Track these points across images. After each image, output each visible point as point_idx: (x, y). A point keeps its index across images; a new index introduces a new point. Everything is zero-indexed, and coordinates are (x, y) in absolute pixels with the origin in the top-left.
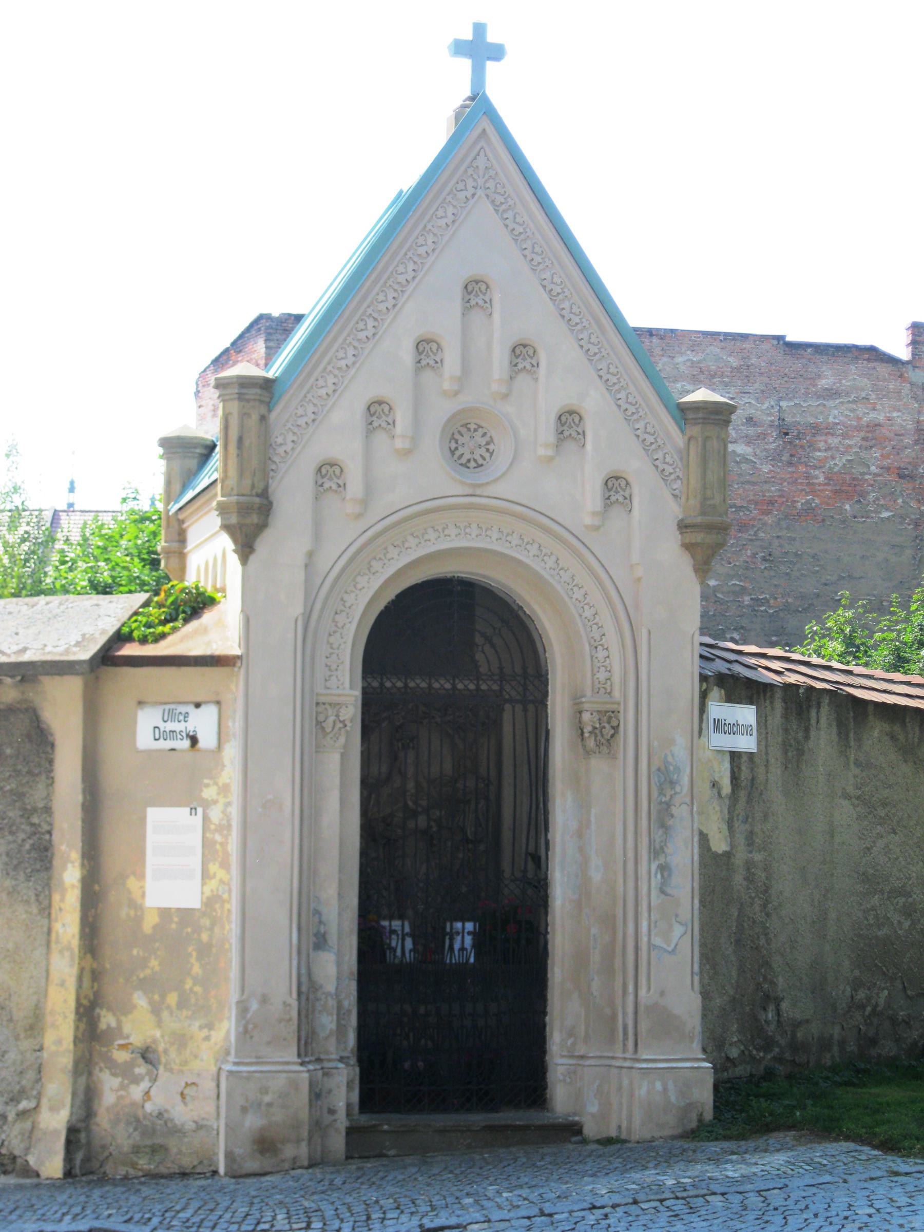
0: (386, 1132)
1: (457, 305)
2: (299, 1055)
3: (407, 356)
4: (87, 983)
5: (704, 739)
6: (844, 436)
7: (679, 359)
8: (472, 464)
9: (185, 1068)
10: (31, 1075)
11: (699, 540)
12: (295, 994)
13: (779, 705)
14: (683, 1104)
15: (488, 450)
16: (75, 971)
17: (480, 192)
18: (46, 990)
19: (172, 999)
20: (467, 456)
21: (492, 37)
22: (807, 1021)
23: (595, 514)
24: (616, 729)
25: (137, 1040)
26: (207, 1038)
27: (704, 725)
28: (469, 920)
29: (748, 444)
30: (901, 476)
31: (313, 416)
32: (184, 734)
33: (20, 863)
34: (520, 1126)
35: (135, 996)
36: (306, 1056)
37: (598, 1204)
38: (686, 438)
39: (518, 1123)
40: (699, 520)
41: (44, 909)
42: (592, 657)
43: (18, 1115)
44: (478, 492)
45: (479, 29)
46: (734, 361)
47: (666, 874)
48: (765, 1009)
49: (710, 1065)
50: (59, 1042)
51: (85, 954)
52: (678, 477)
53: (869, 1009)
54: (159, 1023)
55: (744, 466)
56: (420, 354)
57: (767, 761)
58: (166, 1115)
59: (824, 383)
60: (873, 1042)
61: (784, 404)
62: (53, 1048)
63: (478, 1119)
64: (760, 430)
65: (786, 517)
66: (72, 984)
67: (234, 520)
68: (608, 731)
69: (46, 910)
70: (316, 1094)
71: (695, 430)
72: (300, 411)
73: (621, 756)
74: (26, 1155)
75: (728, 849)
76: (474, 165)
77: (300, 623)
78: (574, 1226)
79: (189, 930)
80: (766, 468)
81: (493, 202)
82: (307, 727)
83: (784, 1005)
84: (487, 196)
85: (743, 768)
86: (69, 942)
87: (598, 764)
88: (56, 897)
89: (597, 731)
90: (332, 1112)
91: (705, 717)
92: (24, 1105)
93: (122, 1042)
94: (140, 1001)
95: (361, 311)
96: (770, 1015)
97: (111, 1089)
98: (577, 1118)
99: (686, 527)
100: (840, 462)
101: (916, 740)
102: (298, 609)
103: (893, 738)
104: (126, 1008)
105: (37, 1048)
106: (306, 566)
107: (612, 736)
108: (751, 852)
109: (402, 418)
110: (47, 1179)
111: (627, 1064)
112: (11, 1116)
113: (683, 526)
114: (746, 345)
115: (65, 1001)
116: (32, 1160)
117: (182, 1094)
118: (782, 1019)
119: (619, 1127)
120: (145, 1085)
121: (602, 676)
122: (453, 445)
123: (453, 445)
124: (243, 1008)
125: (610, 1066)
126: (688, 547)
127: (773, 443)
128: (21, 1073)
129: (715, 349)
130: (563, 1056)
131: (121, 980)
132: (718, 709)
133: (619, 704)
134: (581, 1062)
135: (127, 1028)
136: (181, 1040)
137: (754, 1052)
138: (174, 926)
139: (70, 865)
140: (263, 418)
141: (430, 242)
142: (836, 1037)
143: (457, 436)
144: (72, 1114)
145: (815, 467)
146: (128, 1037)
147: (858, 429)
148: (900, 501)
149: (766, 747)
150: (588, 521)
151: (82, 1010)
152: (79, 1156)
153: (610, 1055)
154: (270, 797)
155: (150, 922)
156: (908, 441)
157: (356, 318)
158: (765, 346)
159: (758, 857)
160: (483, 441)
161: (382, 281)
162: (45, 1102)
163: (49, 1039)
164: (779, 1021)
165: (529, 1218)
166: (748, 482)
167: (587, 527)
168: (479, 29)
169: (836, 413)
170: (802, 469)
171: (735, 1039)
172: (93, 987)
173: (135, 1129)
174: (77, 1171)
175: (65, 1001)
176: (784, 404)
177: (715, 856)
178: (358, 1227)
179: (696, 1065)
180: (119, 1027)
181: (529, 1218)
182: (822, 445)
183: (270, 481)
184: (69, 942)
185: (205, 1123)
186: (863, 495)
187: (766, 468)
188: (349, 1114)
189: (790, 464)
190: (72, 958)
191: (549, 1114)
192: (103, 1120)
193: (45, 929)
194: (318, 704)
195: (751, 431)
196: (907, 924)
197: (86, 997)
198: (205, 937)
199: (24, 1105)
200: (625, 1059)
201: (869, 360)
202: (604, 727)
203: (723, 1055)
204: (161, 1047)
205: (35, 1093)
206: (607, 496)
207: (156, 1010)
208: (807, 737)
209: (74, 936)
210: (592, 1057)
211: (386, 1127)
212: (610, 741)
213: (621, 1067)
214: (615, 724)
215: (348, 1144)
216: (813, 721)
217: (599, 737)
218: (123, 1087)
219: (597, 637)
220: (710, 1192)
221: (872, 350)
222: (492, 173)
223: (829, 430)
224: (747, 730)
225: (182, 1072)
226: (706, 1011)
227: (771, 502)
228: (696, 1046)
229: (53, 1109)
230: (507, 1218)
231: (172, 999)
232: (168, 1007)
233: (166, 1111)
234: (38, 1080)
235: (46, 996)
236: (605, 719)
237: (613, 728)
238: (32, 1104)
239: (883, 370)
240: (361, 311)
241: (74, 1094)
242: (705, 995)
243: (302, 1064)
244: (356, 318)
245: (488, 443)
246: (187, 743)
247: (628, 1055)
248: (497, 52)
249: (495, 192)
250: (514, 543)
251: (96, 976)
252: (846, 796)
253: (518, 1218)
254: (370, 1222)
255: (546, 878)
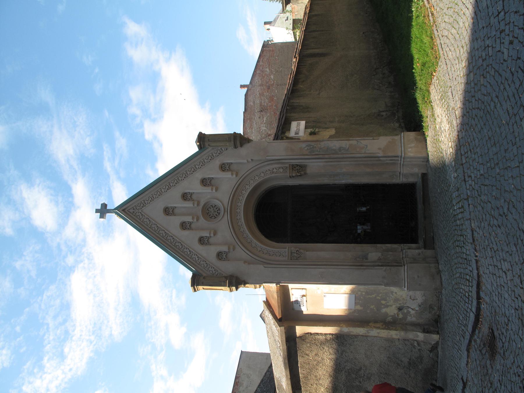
0: (425, 236)
1: (172, 218)
2: (401, 266)
3: (186, 233)
4: (378, 325)
5: (301, 138)
6: (262, 100)
7: (249, 131)
8: (219, 211)
9: (405, 299)
10: (407, 342)
11: (239, 142)
12: (382, 267)
13: (292, 115)
14: (415, 142)
15: (215, 207)
16: (375, 330)
17: (140, 211)
18: (380, 337)
19: (383, 302)
20: (216, 213)
21: (99, 207)
22: (385, 103)
23: (232, 174)
24: (297, 165)
25: (396, 312)
26: (396, 293)
27: (297, 138)
28: (357, 227)
29: (264, 118)
30: (269, 89)
31: (204, 262)
32: (301, 299)
33: (342, 343)
34: (423, 193)
35: (382, 312)
36: (401, 263)
37: (463, 178)
38: (209, 147)
39: (422, 194)
40: (232, 142)
41: (356, 337)
42: (276, 173)
43: (419, 346)
44: (226, 210)
45: (97, 211)
46: (249, 121)
47: (342, 149)
48: (383, 116)
49: (402, 133)
50: (396, 335)
51: (369, 326)
52: (221, 149)
53: (380, 85)
54: (391, 306)
55: (268, 118)
56: (186, 228)
57: (308, 117)
58: (420, 304)
59: (252, 104)
60: (390, 83)
61: (256, 111)
62: (398, 336)
63: (420, 206)
64: (261, 116)
65: (277, 110)
66: (379, 331)
67: (234, 288)
68: (298, 168)
69: (356, 336)
70: (414, 261)
71: (207, 144)
72: (203, 266)
73: (306, 164)
74: (431, 344)
75: (334, 129)
76: (132, 213)
77: (266, 266)
78: (475, 190)
79: (362, 297)
80: (268, 114)
81: (142, 207)
82: (298, 263)
83: (381, 110)
84: (141, 209)
85: (310, 125)
86: (366, 331)
87: (308, 171)
88: (352, 333)
89: (299, 171)
90: (419, 254)
91: (294, 137)
92: (416, 344)
93: (396, 316)
94: (384, 310)
95: (173, 247)
96: (384, 114)
97: (411, 319)
98: (420, 175)
99: (235, 146)
100: (267, 101)
101: (304, 75)
102: (261, 267)
103: (303, 81)
104: (386, 314)
105: (398, 340)
106: (249, 264)
107: (300, 166)
108: (335, 121)
109: (205, 234)
110: (439, 339)
111: (402, 160)
112: (419, 348)
113: (236, 147)
114: (246, 119)
115: (384, 332)
116: (433, 343)
117: (413, 300)
118: (385, 110)
119: (423, 161)
120: (410, 310)
121: (281, 170)
122: (213, 217)
123: (213, 217)
124: (387, 285)
125: (403, 165)
126: (241, 146)
127: (263, 113)
128: (406, 345)
129: (246, 125)
130: (400, 179)
131: (377, 315)
132: (292, 134)
133: (290, 165)
134: (401, 174)
135: (392, 314)
136: (396, 300)
137: (396, 118)
138: (360, 302)
139: (342, 330)
140: (204, 278)
141: (154, 226)
142: (389, 94)
143: (211, 216)
144: (419, 332)
145: (268, 105)
146: (395, 314)
147: (260, 97)
148: (274, 89)
149: (304, 118)
150: (234, 176)
151: (387, 327)
152: (432, 329)
153: (399, 165)
154: (320, 276)
155: (359, 307)
156: (262, 88)
157: (176, 248)
158: (246, 115)
159: (337, 119)
160: (212, 208)
161: (165, 241)
162: (415, 339)
163: (395, 336)
164: (386, 111)
165: (469, 205)
166: (271, 118)
167: (236, 176)
168: (97, 211)
169: (258, 102)
170: (268, 107)
171: (392, 125)
172: (379, 323)
173: (424, 313)
174: (437, 330)
175: (384, 332)
176: (256, 111)
177: (336, 133)
178: (470, 264)
179: (402, 138)
180: (392, 316)
181: (469, 205)
182: (264, 104)
183: (223, 275)
184: (366, 331)
185: (423, 294)
186: (273, 96)
187: (268, 114)
188: (418, 248)
189: (267, 110)
190: (370, 330)
191: (418, 183)
192: (421, 321)
193: (362, 337)
194: (291, 259)
195: (261, 117)
196: (355, 75)
197: (382, 326)
198: (364, 293)
199: (416, 344)
200: (401, 160)
201: (247, 96)
202: (297, 169)
203: (398, 128)
204: (398, 305)
205: (412, 341)
206: (227, 170)
207: (387, 306)
208: (302, 106)
209: (364, 330)
210: (400, 170)
211: (424, 236)
212: (301, 166)
213: (403, 161)
214: (296, 166)
215: (429, 249)
216: (297, 104)
217: (300, 170)
218: (411, 315)
219: (270, 172)
220: (489, 148)
221: (245, 95)
222: (135, 208)
223: (261, 103)
224: (299, 125)
225: (406, 300)
226: (386, 135)
227: (275, 113)
228: (397, 138)
229: (418, 336)
230: (469, 212)
231: (383, 302)
232: (386, 303)
233: (418, 304)
234: (408, 340)
235: (382, 337)
236: (294, 169)
237: (297, 166)
238: (416, 342)
239: (249, 93)
240: (173, 247)
241: (413, 331)
242: (380, 135)
243: (405, 265)
244: (176, 248)
245: (213, 207)
246: (304, 298)
247: (400, 159)
248: (104, 206)
249: (140, 206)
250: (242, 198)
251: (376, 322)
252: (319, 94)
253: (469, 209)
254: (467, 259)
255: (344, 184)
